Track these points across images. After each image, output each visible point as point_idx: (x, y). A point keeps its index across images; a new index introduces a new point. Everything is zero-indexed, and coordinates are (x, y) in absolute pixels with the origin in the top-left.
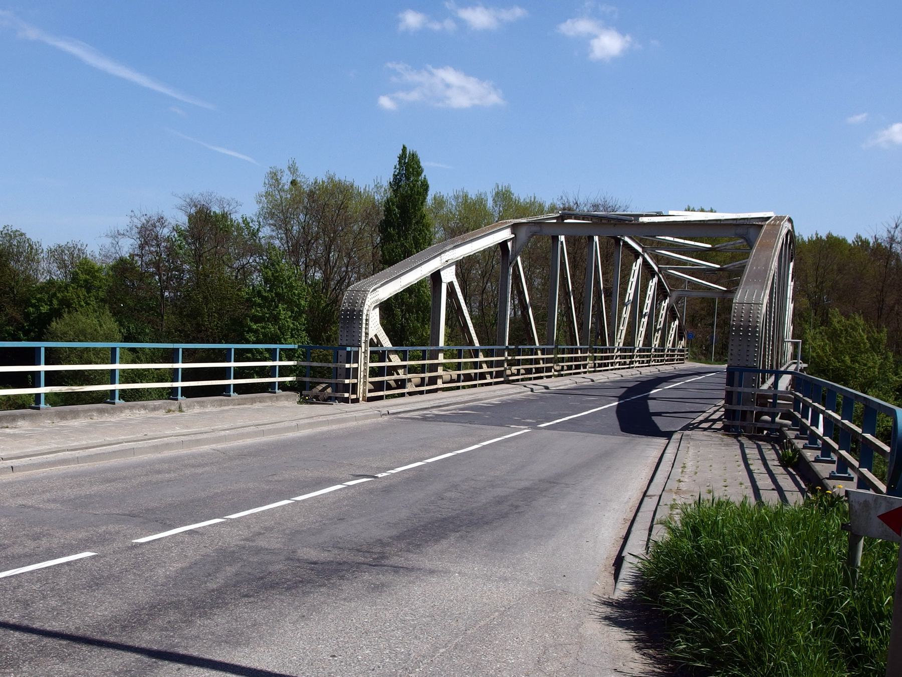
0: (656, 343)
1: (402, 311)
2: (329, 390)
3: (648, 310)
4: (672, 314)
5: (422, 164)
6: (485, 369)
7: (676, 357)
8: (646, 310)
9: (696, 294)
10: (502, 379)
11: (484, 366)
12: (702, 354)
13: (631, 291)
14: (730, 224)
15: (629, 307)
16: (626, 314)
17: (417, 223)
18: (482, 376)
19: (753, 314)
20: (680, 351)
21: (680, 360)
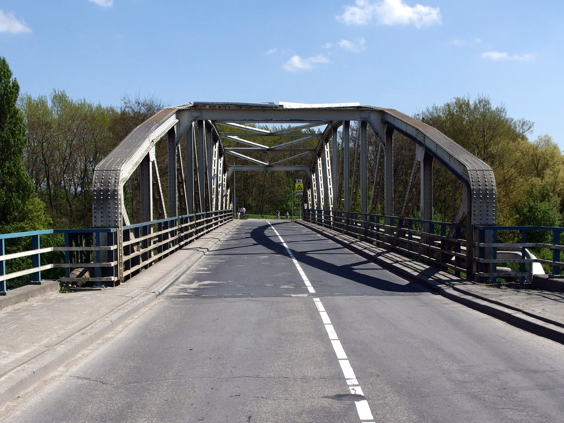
2: (87, 275)
5: (10, 68)
14: (349, 110)
17: (11, 117)
19: (488, 180)
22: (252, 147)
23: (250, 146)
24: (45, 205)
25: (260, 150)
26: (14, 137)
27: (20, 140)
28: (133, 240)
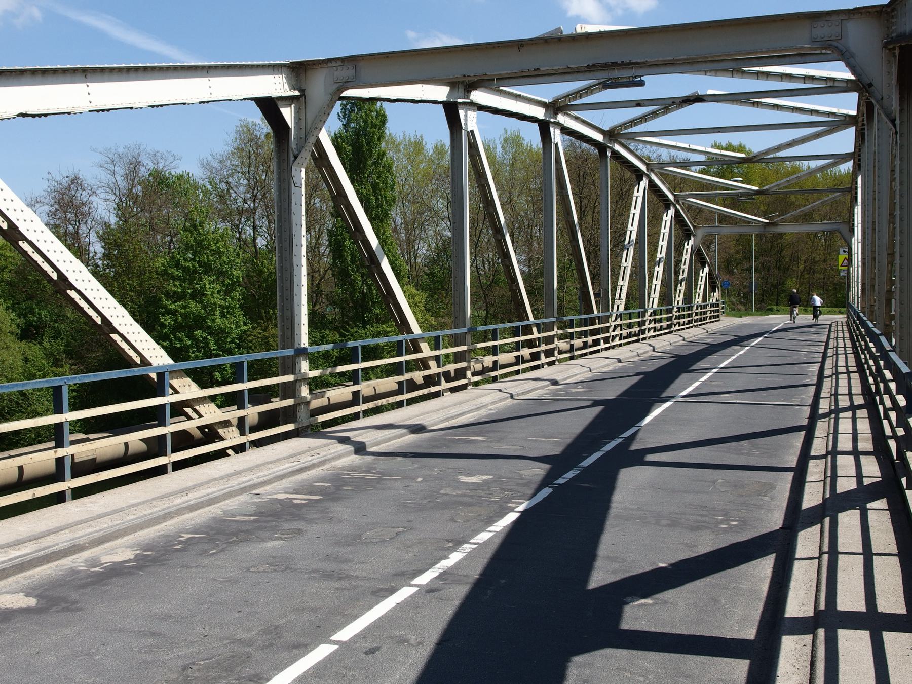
0: (679, 299)
1: (362, 277)
3: (663, 255)
4: (699, 258)
6: (434, 369)
7: (708, 315)
8: (661, 255)
9: (728, 230)
10: (290, 427)
11: (433, 364)
12: (741, 303)
13: (633, 229)
15: (631, 251)
16: (627, 262)
18: (430, 381)
20: (713, 305)
21: (715, 317)
22: (728, 189)
23: (727, 187)
24: (425, 296)
25: (743, 194)
26: (375, 194)
27: (385, 197)
28: (700, 310)
